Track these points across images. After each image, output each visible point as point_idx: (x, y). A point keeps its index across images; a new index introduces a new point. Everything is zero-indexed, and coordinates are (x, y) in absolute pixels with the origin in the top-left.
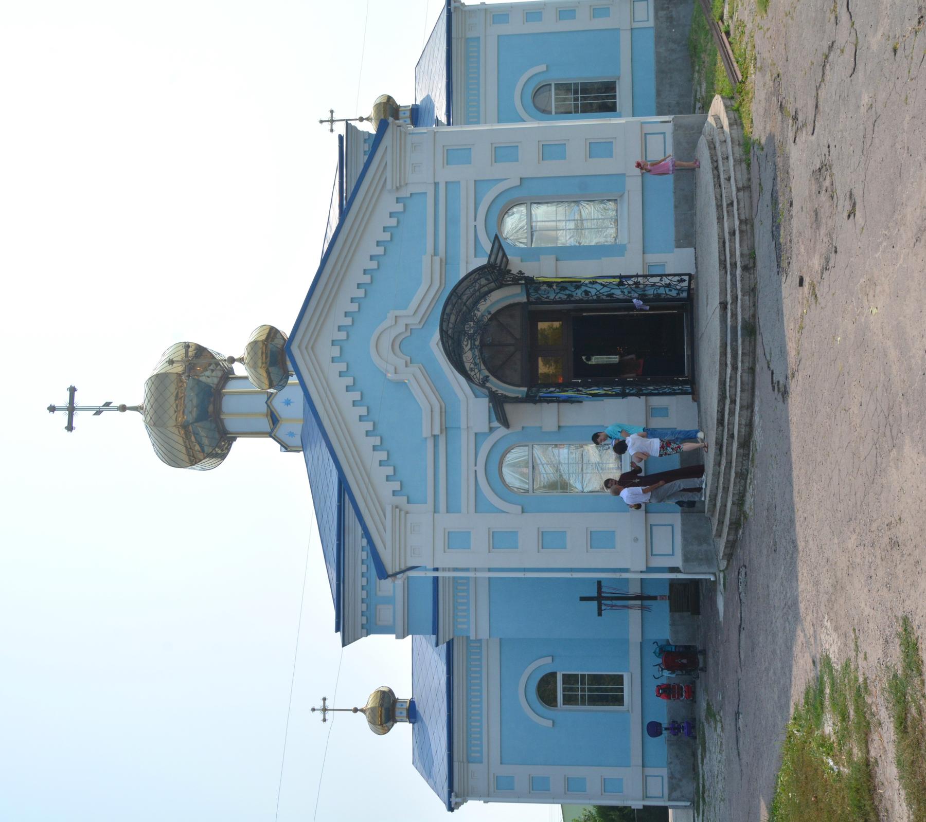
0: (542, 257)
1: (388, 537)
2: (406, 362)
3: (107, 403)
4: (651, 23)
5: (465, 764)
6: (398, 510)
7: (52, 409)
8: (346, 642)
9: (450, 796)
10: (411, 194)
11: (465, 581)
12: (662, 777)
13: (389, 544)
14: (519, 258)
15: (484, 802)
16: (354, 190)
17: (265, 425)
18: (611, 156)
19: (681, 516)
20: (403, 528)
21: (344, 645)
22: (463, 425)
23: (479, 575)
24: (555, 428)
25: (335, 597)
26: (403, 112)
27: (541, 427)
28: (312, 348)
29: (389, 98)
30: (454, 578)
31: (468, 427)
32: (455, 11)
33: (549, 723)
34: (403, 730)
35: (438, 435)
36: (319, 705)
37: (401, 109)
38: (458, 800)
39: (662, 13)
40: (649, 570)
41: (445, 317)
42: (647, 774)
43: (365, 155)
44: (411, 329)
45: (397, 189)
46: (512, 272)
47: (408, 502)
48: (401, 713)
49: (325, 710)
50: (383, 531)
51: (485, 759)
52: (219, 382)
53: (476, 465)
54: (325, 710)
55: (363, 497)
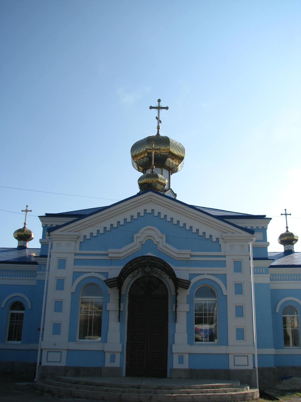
0: (188, 305)
1: (65, 233)
2: (142, 242)
3: (161, 121)
6: (77, 237)
7: (159, 101)
10: (220, 245)
12: (60, 362)
13: (70, 233)
20: (68, 239)
21: (39, 217)
22: (112, 267)
24: (108, 309)
26: (291, 246)
27: (187, 312)
28: (151, 201)
29: (296, 240)
31: (111, 269)
33: (3, 306)
34: (15, 244)
36: (29, 209)
37: (292, 246)
40: (42, 350)
41: (153, 258)
42: (42, 347)
44: (157, 244)
45: (223, 238)
46: (177, 290)
47: (81, 242)
48: (22, 243)
49: (286, 214)
50: (68, 231)
52: (167, 167)
54: (27, 211)
55: (82, 223)
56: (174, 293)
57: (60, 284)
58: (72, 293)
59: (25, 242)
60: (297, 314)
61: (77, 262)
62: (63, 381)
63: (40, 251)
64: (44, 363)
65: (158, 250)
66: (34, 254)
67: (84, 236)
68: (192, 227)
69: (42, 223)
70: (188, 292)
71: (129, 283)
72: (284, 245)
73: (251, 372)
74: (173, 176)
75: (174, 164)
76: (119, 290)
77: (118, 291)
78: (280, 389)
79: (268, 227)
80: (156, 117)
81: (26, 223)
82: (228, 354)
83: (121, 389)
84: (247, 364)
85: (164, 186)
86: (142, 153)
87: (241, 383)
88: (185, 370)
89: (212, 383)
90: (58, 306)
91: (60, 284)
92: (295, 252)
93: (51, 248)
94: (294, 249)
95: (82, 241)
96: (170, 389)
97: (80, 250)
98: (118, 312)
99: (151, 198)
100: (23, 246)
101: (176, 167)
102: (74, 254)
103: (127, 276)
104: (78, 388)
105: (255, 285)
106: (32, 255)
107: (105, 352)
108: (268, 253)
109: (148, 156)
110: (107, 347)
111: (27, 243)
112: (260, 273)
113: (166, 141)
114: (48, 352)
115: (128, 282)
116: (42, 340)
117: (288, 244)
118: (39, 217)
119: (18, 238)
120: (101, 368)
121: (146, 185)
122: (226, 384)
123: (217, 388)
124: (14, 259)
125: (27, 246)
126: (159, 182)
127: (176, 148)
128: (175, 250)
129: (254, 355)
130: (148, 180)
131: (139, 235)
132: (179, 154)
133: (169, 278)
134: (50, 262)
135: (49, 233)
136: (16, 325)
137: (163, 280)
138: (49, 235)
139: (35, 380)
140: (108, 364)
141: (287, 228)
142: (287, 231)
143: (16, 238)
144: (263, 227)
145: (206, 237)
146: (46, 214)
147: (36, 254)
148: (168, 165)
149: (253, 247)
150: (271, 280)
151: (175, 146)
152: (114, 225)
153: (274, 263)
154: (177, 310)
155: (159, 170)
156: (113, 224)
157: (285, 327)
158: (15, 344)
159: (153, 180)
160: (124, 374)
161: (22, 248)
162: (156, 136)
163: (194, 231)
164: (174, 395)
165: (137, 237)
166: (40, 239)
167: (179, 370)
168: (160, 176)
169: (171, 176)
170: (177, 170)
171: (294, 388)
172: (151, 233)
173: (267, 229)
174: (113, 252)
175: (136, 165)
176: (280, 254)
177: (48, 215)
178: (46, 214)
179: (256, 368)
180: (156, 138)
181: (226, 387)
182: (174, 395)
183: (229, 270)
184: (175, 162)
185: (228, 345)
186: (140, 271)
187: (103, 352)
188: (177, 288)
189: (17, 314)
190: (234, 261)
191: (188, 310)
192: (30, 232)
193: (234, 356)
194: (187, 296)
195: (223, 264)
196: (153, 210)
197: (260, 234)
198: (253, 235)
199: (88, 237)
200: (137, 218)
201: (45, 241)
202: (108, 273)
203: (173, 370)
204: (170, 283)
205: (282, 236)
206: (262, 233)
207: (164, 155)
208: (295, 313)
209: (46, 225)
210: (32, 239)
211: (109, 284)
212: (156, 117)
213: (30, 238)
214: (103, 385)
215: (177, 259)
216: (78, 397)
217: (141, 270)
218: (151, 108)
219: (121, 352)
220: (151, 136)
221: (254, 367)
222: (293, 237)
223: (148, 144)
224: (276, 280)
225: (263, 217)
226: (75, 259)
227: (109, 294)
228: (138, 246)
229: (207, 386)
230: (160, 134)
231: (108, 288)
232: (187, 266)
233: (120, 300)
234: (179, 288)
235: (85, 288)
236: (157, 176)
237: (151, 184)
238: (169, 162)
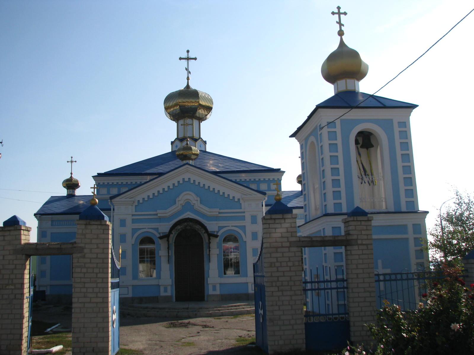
0: (218, 249)
6: (133, 202)
7: (188, 51)
8: (94, 178)
9: (39, 214)
10: (241, 204)
12: (128, 294)
15: (37, 227)
16: (243, 185)
17: (181, 136)
21: (92, 176)
22: (161, 224)
24: (160, 255)
27: (218, 254)
28: (187, 171)
34: (64, 192)
36: (74, 160)
38: (38, 217)
44: (194, 205)
47: (136, 206)
49: (72, 162)
56: (207, 241)
58: (133, 245)
59: (73, 190)
61: (134, 221)
67: (138, 201)
69: (96, 182)
70: (218, 239)
74: (203, 124)
79: (282, 179)
82: (248, 283)
83: (177, 310)
88: (217, 295)
89: (235, 304)
96: (208, 309)
97: (135, 212)
98: (168, 257)
102: (131, 215)
104: (148, 311)
107: (160, 286)
113: (195, 94)
118: (92, 176)
122: (244, 304)
123: (238, 306)
128: (207, 209)
140: (163, 294)
144: (278, 179)
146: (98, 173)
152: (160, 191)
154: (210, 253)
161: (71, 196)
164: (210, 312)
167: (213, 295)
168: (193, 148)
173: (281, 180)
174: (161, 213)
177: (100, 175)
178: (98, 173)
181: (244, 305)
182: (210, 312)
187: (159, 286)
188: (209, 239)
190: (251, 216)
194: (217, 243)
195: (243, 218)
196: (189, 179)
199: (141, 201)
202: (158, 228)
209: (99, 183)
210: (80, 186)
214: (164, 308)
215: (208, 216)
216: (150, 317)
226: (132, 219)
227: (160, 244)
229: (231, 305)
230: (189, 84)
233: (168, 248)
236: (190, 149)
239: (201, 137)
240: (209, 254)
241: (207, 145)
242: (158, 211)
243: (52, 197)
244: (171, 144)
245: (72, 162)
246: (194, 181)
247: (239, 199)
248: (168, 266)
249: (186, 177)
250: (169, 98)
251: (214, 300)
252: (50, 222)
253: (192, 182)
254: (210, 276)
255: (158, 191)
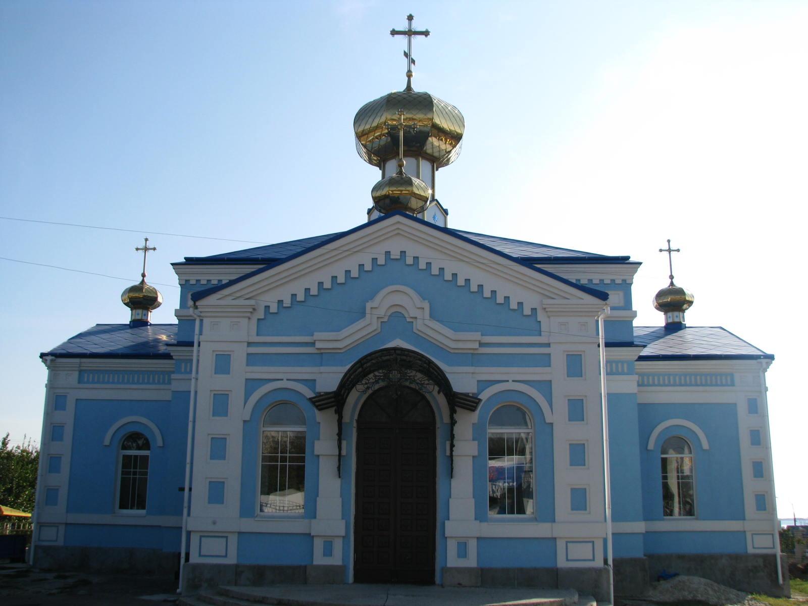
1: (228, 301)
2: (382, 318)
3: (414, 61)
4: (751, 550)
5: (77, 369)
6: (251, 310)
7: (410, 18)
10: (540, 322)
11: (188, 370)
12: (226, 556)
13: (222, 302)
14: (476, 421)
15: (46, 384)
18: (572, 509)
19: (233, 565)
21: (172, 264)
22: (323, 369)
23: (193, 381)
24: (316, 453)
25: (218, 257)
26: (678, 315)
27: (474, 457)
28: (398, 234)
29: (690, 303)
30: (192, 360)
31: (321, 373)
32: (758, 362)
33: (107, 442)
34: (124, 316)
35: (315, 347)
36: (150, 245)
37: (681, 314)
38: (48, 362)
39: (761, 562)
40: (189, 533)
42: (189, 529)
43: (576, 280)
44: (413, 322)
46: (454, 415)
47: (259, 320)
48: (138, 314)
49: (669, 251)
51: (81, 386)
53: (287, 380)
54: (146, 249)
56: (447, 419)
57: (221, 403)
58: (245, 422)
59: (145, 312)
60: (690, 453)
62: (233, 597)
63: (176, 329)
64: (194, 559)
65: (415, 333)
66: (163, 336)
68: (482, 285)
70: (475, 417)
71: (358, 399)
72: (666, 312)
73: (598, 571)
75: (443, 150)
76: (339, 415)
77: (336, 417)
78: (655, 600)
79: (634, 280)
80: (405, 52)
81: (146, 274)
82: (555, 539)
84: (591, 558)
85: (424, 203)
86: (377, 127)
87: (580, 595)
89: (520, 599)
90: (218, 448)
91: (221, 403)
92: (686, 327)
93: (201, 333)
94: (684, 321)
95: (262, 317)
97: (258, 335)
99: (400, 227)
100: (141, 319)
101: (445, 155)
102: (246, 344)
103: (354, 385)
105: (609, 396)
106: (159, 339)
107: (313, 536)
108: (634, 329)
109: (389, 133)
110: (318, 527)
111: (149, 313)
112: (618, 373)
113: (425, 102)
114: (201, 537)
115: (355, 399)
116: (189, 514)
117: (673, 310)
118: (172, 264)
119: (130, 304)
120: (305, 567)
121: (387, 201)
124: (125, 347)
125: (149, 319)
126: (415, 194)
127: (446, 116)
129: (605, 541)
130: (392, 191)
131: (375, 304)
132: (452, 128)
133: (439, 393)
134: (198, 356)
135: (195, 303)
136: (134, 479)
137: (428, 396)
138: (196, 307)
139: (178, 591)
140: (319, 559)
141: (672, 277)
142: (672, 284)
143: (126, 304)
145: (511, 307)
146: (185, 258)
147: (169, 336)
148: (429, 151)
149: (604, 321)
150: (639, 385)
151: (444, 113)
153: (646, 352)
154: (454, 453)
155: (412, 161)
156: (322, 283)
157: (665, 478)
158: (133, 516)
159: (401, 191)
160: (351, 579)
161: (139, 323)
162: (404, 91)
163: (487, 294)
165: (371, 308)
166: (176, 310)
168: (416, 181)
169: (437, 173)
170: (448, 160)
171: (681, 598)
172: (398, 299)
174: (324, 339)
175: (364, 150)
176: (657, 330)
177: (190, 261)
178: (185, 258)
179: (610, 566)
180: (405, 96)
183: (557, 372)
184: (444, 146)
185: (554, 521)
186: (379, 379)
187: (309, 537)
188: (453, 412)
189: (136, 457)
191: (476, 454)
192: (154, 291)
193: (567, 542)
195: (545, 361)
196: (403, 253)
197: (618, 294)
198: (606, 301)
200: (371, 269)
201: (185, 312)
203: (445, 570)
204: (440, 401)
205: (661, 294)
206: (621, 294)
207: (421, 132)
208: (686, 450)
209: (187, 281)
211: (317, 404)
212: (405, 52)
213: (156, 303)
215: (452, 351)
217: (382, 377)
218: (394, 33)
219: (343, 537)
220: (394, 93)
221: (606, 561)
222: (683, 297)
223: (389, 109)
224: (648, 385)
225: (623, 260)
226: (248, 354)
227: (319, 423)
228: (375, 326)
231: (316, 411)
232: (472, 366)
233: (340, 434)
234: (458, 409)
235: (270, 409)
236: (410, 183)
237: (398, 197)
238: (432, 145)
239: (436, 198)
240: (451, 456)
241: (449, 217)
242: (315, 334)
243: (97, 325)
244: (368, 213)
245: (146, 247)
246: (416, 259)
247: (534, 310)
248: (338, 482)
249: (395, 247)
250: (363, 115)
251: (459, 584)
252: (76, 374)
253: (410, 261)
254: (452, 497)
255: (320, 284)
